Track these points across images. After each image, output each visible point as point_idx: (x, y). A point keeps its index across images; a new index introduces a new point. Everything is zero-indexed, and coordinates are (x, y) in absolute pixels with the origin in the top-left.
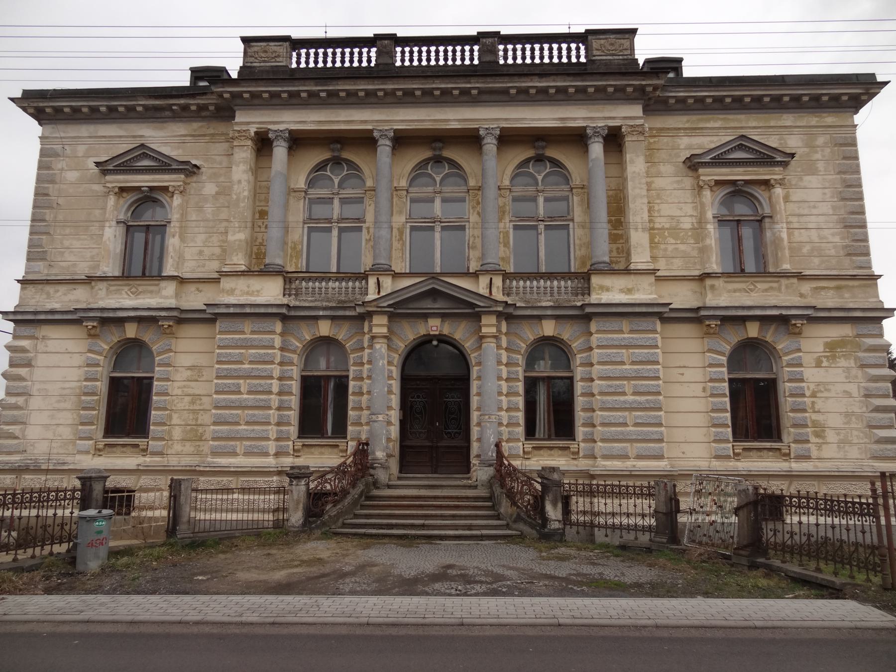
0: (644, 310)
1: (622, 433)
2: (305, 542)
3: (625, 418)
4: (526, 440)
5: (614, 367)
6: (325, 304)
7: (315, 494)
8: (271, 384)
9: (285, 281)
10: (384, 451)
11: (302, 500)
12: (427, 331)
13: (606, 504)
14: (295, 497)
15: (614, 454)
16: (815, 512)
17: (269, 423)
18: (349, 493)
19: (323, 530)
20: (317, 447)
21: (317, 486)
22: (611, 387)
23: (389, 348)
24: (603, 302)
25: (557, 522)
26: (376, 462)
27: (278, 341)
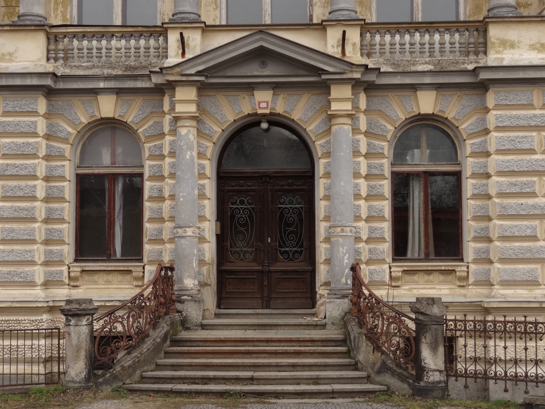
0: (18, 82)
1: (530, 250)
2: (90, 402)
3: (534, 228)
4: (394, 260)
5: (520, 157)
6: (106, 72)
7: (102, 338)
8: (35, 186)
9: (48, 39)
10: (195, 278)
12: (253, 108)
13: (505, 348)
14: (75, 342)
15: (518, 278)
16: (513, 335)
17: (33, 241)
18: (148, 336)
19: (115, 386)
20: (102, 274)
21: (104, 327)
22: (515, 185)
23: (200, 133)
24: (505, 63)
25: (437, 373)
26: (184, 293)
27: (41, 126)
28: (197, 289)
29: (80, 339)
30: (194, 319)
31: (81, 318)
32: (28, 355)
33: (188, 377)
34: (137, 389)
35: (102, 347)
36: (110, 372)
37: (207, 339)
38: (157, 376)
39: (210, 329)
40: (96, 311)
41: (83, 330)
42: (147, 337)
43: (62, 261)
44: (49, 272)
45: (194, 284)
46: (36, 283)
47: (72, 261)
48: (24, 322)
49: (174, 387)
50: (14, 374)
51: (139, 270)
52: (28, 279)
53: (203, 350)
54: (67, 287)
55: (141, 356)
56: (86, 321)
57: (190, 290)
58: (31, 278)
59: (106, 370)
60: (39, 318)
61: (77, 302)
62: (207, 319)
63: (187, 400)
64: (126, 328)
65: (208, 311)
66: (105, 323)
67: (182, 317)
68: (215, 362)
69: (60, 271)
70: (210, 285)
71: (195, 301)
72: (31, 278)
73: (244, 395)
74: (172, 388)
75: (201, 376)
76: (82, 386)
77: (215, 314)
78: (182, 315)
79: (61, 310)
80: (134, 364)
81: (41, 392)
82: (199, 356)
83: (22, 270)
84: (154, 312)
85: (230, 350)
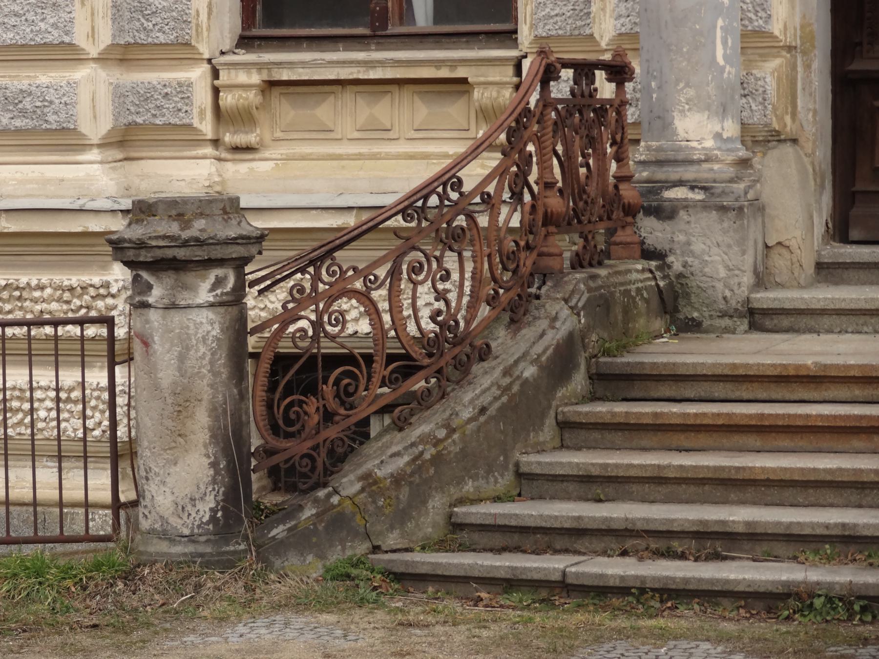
2: (222, 620)
7: (281, 362)
10: (723, 111)
11: (204, 387)
14: (167, 375)
18: (485, 353)
19: (336, 556)
20: (348, 96)
21: (288, 317)
26: (674, 173)
28: (730, 158)
29: (189, 363)
30: (719, 286)
31: (189, 278)
32: (72, 427)
33: (639, 526)
34: (423, 570)
35: (284, 396)
36: (316, 501)
37: (741, 372)
38: (513, 523)
39: (787, 330)
40: (254, 250)
41: (199, 325)
42: (482, 359)
43: (187, 44)
44: (134, 89)
45: (718, 136)
46: (83, 136)
47: (227, 45)
48: (37, 294)
49: (573, 569)
50: (74, 505)
51: (497, 79)
52: (51, 118)
53: (719, 415)
54: (209, 150)
55: (448, 436)
56: (212, 290)
57: (699, 162)
58: (63, 116)
59: (305, 492)
60: (96, 280)
61: (174, 213)
62: (780, 285)
63: (622, 622)
64: (387, 318)
65: (784, 251)
66: (294, 299)
67: (664, 277)
68: (763, 469)
69: (180, 84)
70: (795, 141)
71: (723, 209)
72: (63, 116)
73: (864, 609)
74: (564, 573)
75: (693, 522)
76: (202, 555)
77: (820, 266)
78: (665, 266)
79: (111, 242)
80: (419, 470)
81: (38, 574)
82: (703, 439)
83: (26, 82)
84: (512, 256)
85: (835, 417)
